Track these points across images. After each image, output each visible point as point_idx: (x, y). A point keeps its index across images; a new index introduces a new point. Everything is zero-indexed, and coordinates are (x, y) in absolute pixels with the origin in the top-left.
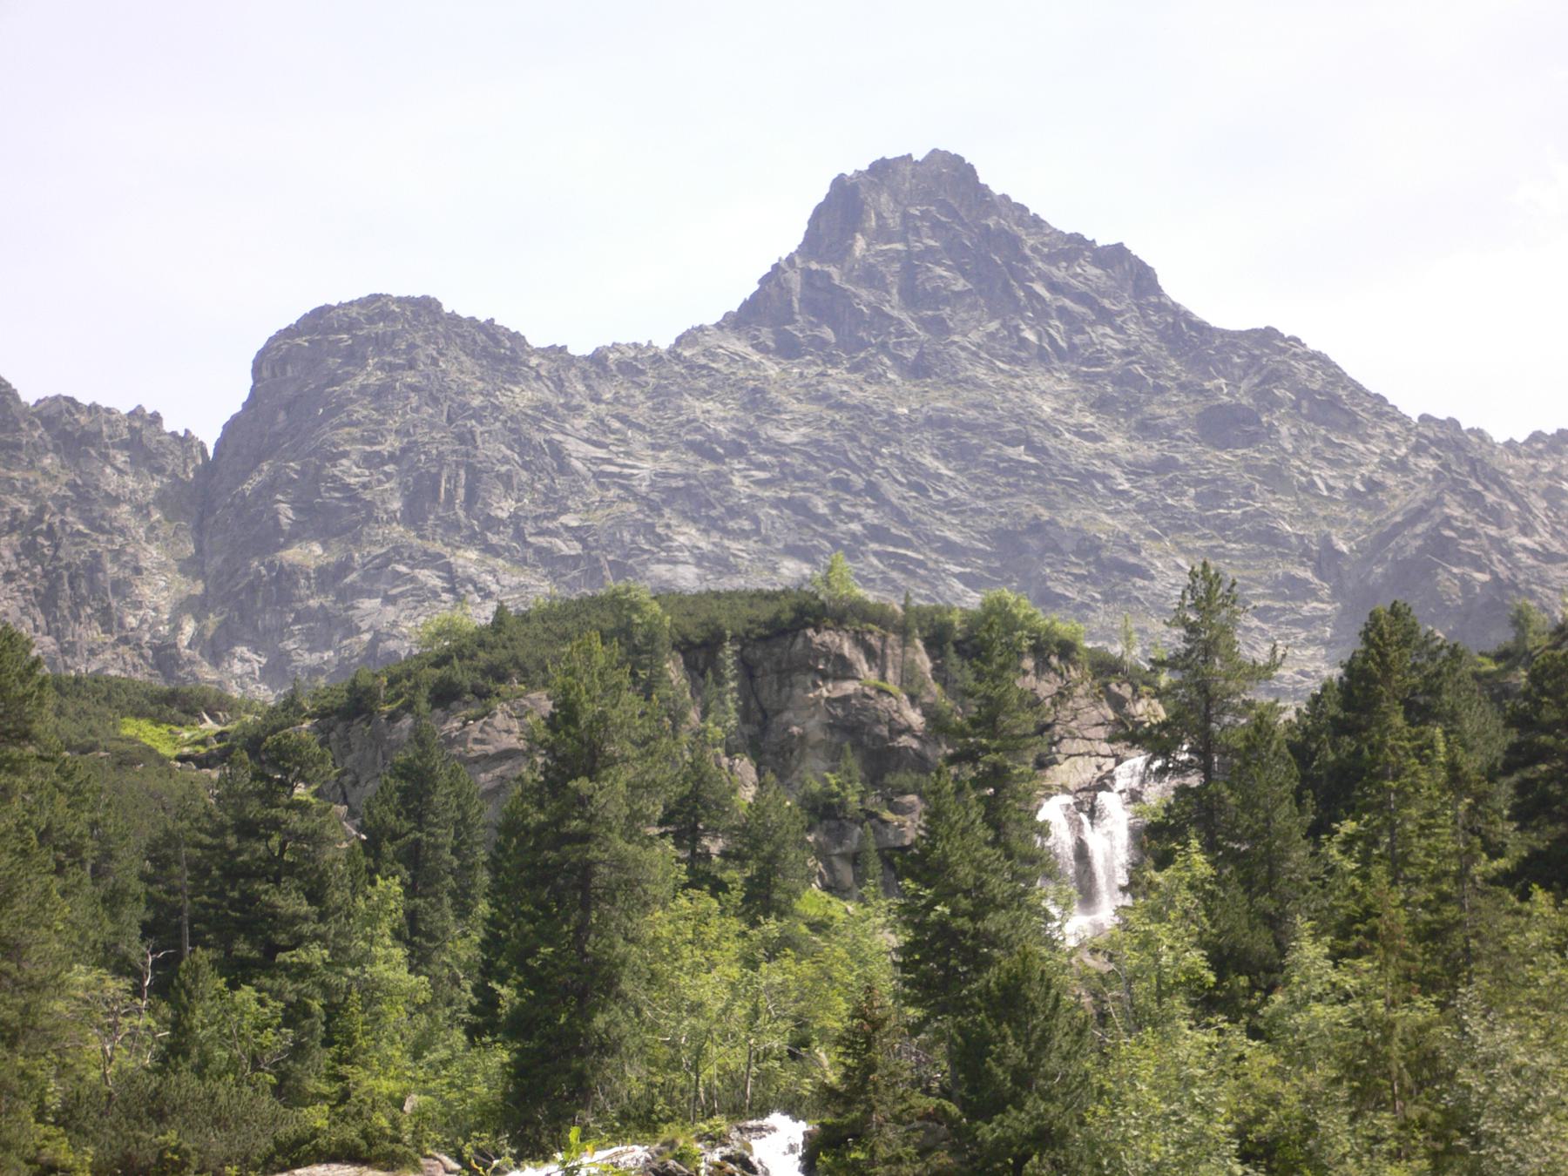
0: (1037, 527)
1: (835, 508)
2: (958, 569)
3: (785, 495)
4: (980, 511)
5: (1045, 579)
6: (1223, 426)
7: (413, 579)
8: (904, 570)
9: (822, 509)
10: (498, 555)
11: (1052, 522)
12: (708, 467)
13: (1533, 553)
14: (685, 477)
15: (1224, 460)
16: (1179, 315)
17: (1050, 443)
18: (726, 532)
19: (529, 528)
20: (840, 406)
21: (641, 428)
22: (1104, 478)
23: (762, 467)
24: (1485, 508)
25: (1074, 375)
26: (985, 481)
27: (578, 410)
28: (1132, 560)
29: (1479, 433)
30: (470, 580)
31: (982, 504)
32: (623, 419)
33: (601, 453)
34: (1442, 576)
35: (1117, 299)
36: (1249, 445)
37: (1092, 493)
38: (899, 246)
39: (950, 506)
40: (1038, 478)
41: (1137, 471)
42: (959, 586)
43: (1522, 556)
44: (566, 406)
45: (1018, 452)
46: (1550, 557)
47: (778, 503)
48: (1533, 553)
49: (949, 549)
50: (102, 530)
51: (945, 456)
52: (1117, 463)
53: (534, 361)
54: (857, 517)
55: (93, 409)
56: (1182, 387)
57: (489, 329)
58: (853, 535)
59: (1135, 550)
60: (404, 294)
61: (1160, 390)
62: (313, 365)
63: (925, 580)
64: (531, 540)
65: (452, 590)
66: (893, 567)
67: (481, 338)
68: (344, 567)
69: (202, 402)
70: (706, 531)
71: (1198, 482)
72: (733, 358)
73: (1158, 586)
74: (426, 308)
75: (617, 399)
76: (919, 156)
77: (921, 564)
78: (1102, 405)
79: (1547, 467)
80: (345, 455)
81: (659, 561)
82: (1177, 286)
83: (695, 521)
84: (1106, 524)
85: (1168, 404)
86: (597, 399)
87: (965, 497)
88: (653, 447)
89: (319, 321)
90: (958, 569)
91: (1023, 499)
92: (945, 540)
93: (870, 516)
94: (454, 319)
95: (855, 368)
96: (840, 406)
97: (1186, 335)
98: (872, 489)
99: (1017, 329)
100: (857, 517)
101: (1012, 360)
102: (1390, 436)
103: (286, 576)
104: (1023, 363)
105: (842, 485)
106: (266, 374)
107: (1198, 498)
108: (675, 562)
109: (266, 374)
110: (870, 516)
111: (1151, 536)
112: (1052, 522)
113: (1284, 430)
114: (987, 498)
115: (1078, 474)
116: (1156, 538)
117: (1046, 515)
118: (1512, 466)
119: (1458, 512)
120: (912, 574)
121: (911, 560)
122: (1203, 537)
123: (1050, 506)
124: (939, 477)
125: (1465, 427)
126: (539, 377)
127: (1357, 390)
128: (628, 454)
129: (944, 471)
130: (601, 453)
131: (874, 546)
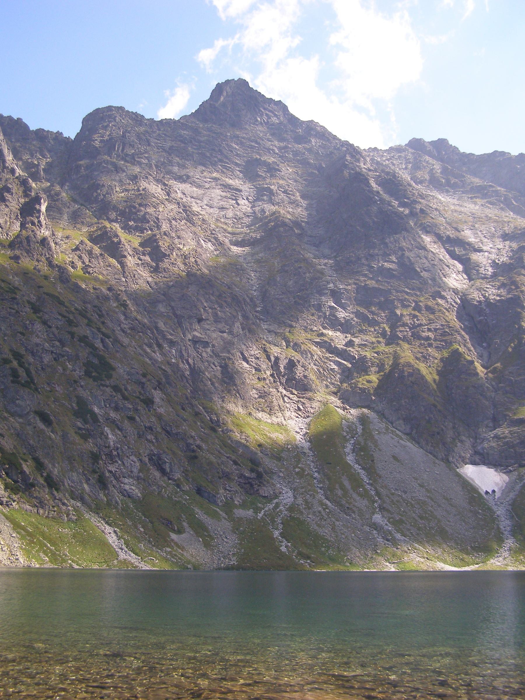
0: (257, 160)
1: (211, 155)
2: (238, 169)
3: (200, 152)
4: (244, 156)
5: (258, 171)
6: (299, 139)
7: (108, 168)
8: (226, 169)
9: (208, 155)
10: (128, 163)
11: (260, 159)
12: (183, 145)
13: (366, 169)
14: (177, 147)
15: (299, 147)
16: (292, 115)
17: (261, 142)
18: (186, 159)
19: (136, 157)
20: (215, 133)
21: (169, 137)
22: (273, 150)
23: (196, 145)
24: (356, 159)
25: (268, 128)
26: (246, 150)
27: (155, 132)
28: (277, 167)
29: (358, 147)
30: (121, 168)
31: (245, 155)
32: (165, 135)
33: (159, 142)
34: (345, 172)
35: (278, 112)
36: (305, 144)
37: (270, 153)
38: (231, 99)
39: (237, 155)
40: (258, 149)
41: (280, 148)
42: (238, 173)
43: (364, 170)
44: (152, 131)
45: (253, 144)
46: (370, 170)
47: (198, 153)
48: (366, 169)
49: (237, 165)
50: (45, 158)
51: (237, 144)
52: (276, 147)
53: (145, 122)
54: (217, 157)
55: (48, 131)
56: (291, 131)
57: (136, 114)
58: (215, 161)
59: (278, 165)
60: (116, 106)
61: (286, 131)
62: (96, 120)
63: (231, 171)
64: (137, 159)
65: (116, 170)
66: (224, 168)
67: (134, 116)
68: (92, 164)
69: (71, 130)
70: (181, 159)
71: (293, 151)
72: (192, 122)
73: (283, 174)
74: (121, 108)
75: (164, 130)
76: (236, 79)
77: (230, 168)
78: (273, 134)
79: (372, 154)
80: (96, 140)
81: (169, 165)
82: (292, 110)
83: (179, 157)
84: (271, 160)
85: (288, 135)
86: (159, 130)
87: (241, 153)
88: (171, 140)
89: (97, 111)
90: (238, 169)
91: (254, 154)
92: (236, 162)
93: (219, 157)
94: (128, 111)
95: (219, 125)
96: (215, 133)
97: (293, 120)
98: (220, 151)
99: (256, 118)
100: (217, 157)
101: (254, 124)
102: (336, 143)
103: (79, 167)
104: (257, 125)
105: (214, 150)
106: (85, 123)
107: (293, 155)
108: (173, 166)
109: (85, 123)
110: (219, 157)
111: (281, 162)
112: (260, 159)
113: (313, 141)
114: (246, 154)
115: (266, 149)
116: (283, 163)
117: (259, 157)
118: (364, 153)
119: (349, 158)
120: (228, 170)
121: (228, 167)
122: (293, 163)
123: (260, 155)
124: (236, 149)
125: (355, 146)
126: (146, 125)
127: (330, 134)
128: (165, 142)
129: (237, 147)
130: (159, 142)
131: (220, 163)
